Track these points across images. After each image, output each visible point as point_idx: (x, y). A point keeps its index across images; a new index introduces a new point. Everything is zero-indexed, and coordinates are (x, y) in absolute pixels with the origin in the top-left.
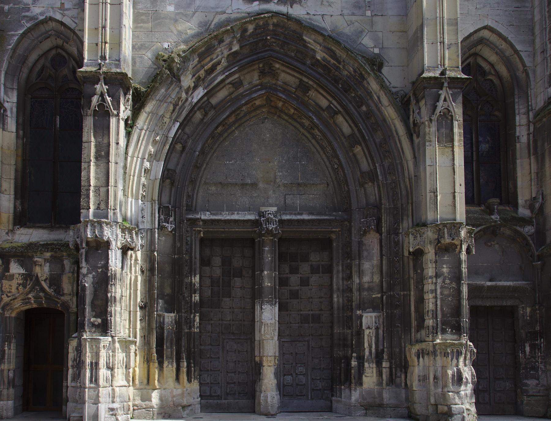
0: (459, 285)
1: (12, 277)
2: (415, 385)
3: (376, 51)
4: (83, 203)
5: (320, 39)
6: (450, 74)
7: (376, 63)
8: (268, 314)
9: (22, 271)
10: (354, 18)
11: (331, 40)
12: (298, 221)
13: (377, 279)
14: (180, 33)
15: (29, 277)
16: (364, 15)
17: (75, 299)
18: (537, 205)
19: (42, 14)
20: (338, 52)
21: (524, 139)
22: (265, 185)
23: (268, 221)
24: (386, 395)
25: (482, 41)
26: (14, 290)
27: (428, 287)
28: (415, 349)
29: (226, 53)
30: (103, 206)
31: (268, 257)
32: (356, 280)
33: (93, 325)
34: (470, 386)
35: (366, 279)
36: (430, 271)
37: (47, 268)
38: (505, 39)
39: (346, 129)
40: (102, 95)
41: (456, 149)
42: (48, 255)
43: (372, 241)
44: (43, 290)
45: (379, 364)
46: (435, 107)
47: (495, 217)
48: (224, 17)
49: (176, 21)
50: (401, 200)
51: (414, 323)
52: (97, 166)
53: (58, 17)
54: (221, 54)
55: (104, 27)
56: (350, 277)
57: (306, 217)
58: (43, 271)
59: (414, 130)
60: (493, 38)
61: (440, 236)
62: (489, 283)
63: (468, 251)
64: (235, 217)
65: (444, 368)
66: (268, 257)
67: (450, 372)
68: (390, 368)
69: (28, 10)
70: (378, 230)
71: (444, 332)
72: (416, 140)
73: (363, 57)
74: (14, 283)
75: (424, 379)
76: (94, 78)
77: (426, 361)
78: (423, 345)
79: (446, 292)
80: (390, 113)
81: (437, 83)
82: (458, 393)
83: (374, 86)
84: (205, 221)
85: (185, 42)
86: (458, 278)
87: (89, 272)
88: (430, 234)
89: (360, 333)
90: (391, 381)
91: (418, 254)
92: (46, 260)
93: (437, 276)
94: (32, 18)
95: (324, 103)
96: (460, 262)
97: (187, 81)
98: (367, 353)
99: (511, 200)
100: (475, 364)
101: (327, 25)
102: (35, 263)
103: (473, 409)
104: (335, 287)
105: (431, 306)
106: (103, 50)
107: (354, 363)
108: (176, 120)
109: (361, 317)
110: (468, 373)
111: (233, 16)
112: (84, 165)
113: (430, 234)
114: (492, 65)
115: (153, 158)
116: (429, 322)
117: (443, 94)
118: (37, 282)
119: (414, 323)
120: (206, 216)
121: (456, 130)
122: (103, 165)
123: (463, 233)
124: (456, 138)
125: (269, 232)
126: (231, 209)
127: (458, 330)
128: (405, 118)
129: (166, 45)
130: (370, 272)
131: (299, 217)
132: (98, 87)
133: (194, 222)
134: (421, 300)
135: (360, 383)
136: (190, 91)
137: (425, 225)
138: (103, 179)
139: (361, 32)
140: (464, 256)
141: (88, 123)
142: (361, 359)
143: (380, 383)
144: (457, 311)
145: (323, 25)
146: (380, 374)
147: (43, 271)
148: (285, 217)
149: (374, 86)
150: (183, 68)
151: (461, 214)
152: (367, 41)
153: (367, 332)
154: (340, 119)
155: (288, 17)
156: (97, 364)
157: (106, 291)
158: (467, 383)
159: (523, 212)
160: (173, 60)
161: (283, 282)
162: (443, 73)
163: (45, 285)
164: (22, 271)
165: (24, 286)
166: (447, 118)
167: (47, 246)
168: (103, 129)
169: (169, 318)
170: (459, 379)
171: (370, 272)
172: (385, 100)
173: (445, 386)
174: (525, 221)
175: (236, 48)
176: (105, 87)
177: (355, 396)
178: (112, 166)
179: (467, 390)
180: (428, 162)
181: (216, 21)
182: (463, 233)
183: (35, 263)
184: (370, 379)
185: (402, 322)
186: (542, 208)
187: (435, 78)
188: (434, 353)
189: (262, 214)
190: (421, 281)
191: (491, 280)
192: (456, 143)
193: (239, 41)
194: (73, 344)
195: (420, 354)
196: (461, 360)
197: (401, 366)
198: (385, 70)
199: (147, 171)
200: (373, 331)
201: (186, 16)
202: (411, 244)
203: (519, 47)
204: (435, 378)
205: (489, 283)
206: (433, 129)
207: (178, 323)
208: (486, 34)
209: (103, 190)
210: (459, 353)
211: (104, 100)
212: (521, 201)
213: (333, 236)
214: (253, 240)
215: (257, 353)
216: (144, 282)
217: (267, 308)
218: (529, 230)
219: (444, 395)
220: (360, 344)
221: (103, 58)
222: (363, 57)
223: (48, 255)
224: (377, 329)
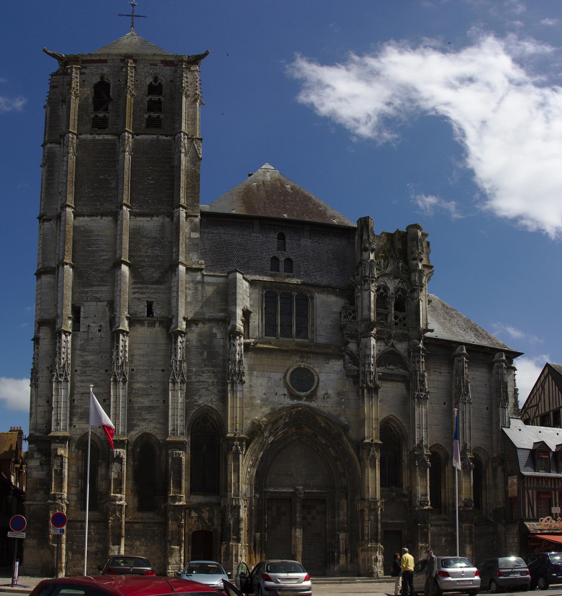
0: (377, 524)
1: (192, 518)
2: (361, 563)
3: (346, 423)
4: (229, 489)
5: (324, 419)
6: (376, 441)
7: (346, 429)
8: (299, 533)
9: (197, 515)
10: (337, 408)
11: (327, 418)
12: (312, 492)
13: (346, 519)
14: (263, 412)
15: (200, 518)
16: (341, 407)
17: (220, 527)
18: (410, 490)
19: (203, 403)
20: (330, 424)
21: (406, 461)
22: (299, 478)
23: (300, 493)
24: (349, 567)
25: (390, 419)
26: (193, 523)
27: (366, 524)
28: (360, 549)
29: (283, 422)
30: (237, 491)
31: (299, 508)
32: (337, 519)
33: (233, 539)
34: (381, 563)
35: (341, 518)
36: (367, 519)
37: (207, 514)
38: (399, 421)
39: (333, 453)
40: (236, 446)
41: (377, 471)
42: (208, 508)
43: (344, 502)
44: (205, 523)
45: (346, 555)
46: (369, 454)
47: (394, 494)
48: (282, 406)
49: (261, 407)
50: (357, 486)
51: (361, 538)
52: (234, 474)
53: (210, 405)
54: (281, 423)
55: (236, 417)
56: (334, 517)
57: (315, 491)
58: (206, 515)
59: (361, 460)
60: (394, 419)
61: (371, 505)
62: (390, 521)
63: (381, 510)
64: (284, 490)
65: (371, 556)
66: (299, 508)
67: (373, 557)
68: (351, 556)
69: (197, 402)
70: (347, 498)
71: (371, 542)
72: (362, 464)
73: (341, 426)
74: (193, 521)
75: (364, 560)
76: (233, 439)
77: (365, 553)
78: (364, 547)
79: (372, 527)
80: (352, 451)
81: (370, 444)
82: (376, 565)
83: (345, 439)
84: (271, 492)
85: (265, 417)
86: (376, 521)
87: (232, 518)
88: (366, 504)
89: (338, 541)
90: (351, 561)
91: (362, 511)
92: (206, 511)
93: (369, 520)
94: (199, 405)
95: (324, 442)
96: (378, 515)
97: (266, 434)
98: (341, 550)
99: (400, 485)
100: (383, 554)
101: (326, 410)
102: (203, 512)
103: (382, 572)
104: (327, 521)
105: (367, 532)
106: (236, 427)
107: (336, 554)
108: (261, 450)
109: (339, 535)
110: (380, 557)
111: (286, 406)
112: (229, 474)
113: (366, 504)
114: (394, 428)
115: (252, 466)
116: (366, 538)
117: (372, 449)
118: (204, 520)
119: (361, 538)
120: (272, 490)
121: (377, 463)
122: (236, 474)
123: (379, 504)
124: (377, 466)
125: (300, 498)
126: (283, 487)
127: (377, 541)
128: (358, 454)
129: (257, 418)
130: (343, 516)
131: (312, 491)
132: (235, 443)
133: (266, 492)
134: (363, 529)
135: (338, 563)
136: (267, 438)
137: (365, 500)
138: (237, 480)
139: (340, 415)
140: (379, 512)
141: (230, 457)
142: (339, 553)
143: (346, 562)
144: (376, 534)
145: (324, 411)
146: (347, 559)
147: (206, 515)
148: (307, 491)
149: (345, 439)
150: (265, 429)
151: (378, 496)
152: (342, 419)
153: (341, 541)
154: (330, 449)
155: (309, 407)
156: (237, 554)
157: (239, 525)
158: (380, 561)
159: (405, 492)
160: (261, 426)
161: (304, 518)
162: (372, 441)
163: (207, 521)
164: (197, 515)
165: (198, 522)
166: (373, 459)
167: (206, 504)
168: (236, 460)
169: (258, 534)
170: (376, 560)
171: (343, 516)
172: (350, 445)
173: (371, 562)
174: (405, 496)
175: (287, 420)
176: (238, 443)
177: (336, 568)
178: (240, 474)
179: (380, 564)
180: (366, 475)
181: (278, 407)
182: (379, 504)
183: (203, 512)
184: (342, 561)
185: (356, 538)
186: (411, 490)
187: (369, 443)
188: (368, 550)
189: (297, 490)
190: (363, 521)
191: (392, 520)
192: (377, 468)
193: (289, 418)
194: (224, 547)
195: (363, 550)
196: (378, 553)
197: (355, 555)
198: (350, 431)
199: (249, 472)
200: (344, 541)
201: (265, 405)
202: (359, 507)
203: (404, 424)
204: (368, 559)
205: (390, 521)
206: (368, 462)
207: (261, 536)
208: (392, 417)
209: (237, 484)
210: (377, 550)
211: (237, 448)
212: (404, 487)
213: (327, 498)
214: (291, 499)
215: (293, 550)
216: (248, 519)
217: (298, 530)
218: (406, 500)
219: (371, 566)
220: (339, 546)
221: (236, 430)
222: (341, 426)
223: (208, 508)
224: (346, 540)
